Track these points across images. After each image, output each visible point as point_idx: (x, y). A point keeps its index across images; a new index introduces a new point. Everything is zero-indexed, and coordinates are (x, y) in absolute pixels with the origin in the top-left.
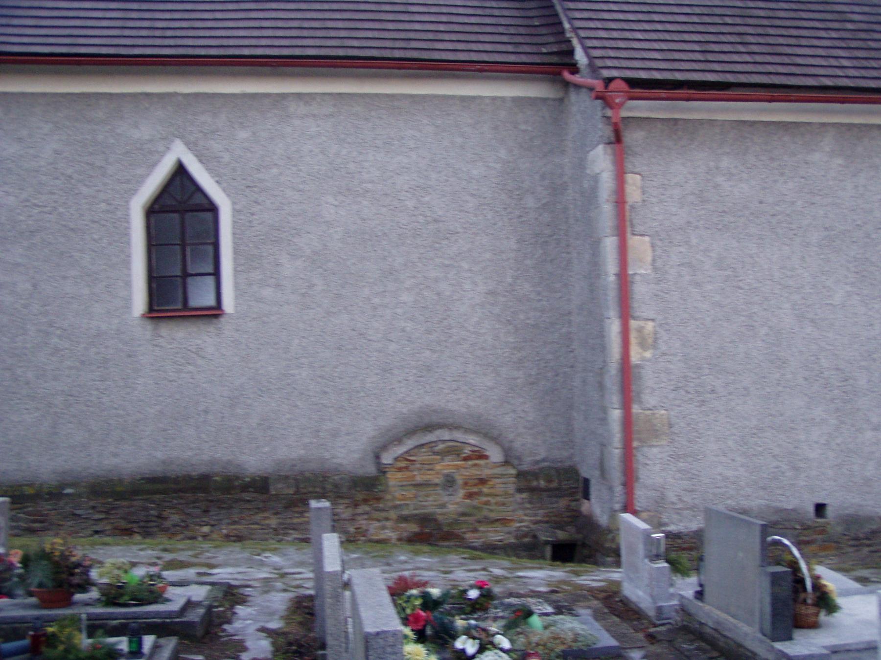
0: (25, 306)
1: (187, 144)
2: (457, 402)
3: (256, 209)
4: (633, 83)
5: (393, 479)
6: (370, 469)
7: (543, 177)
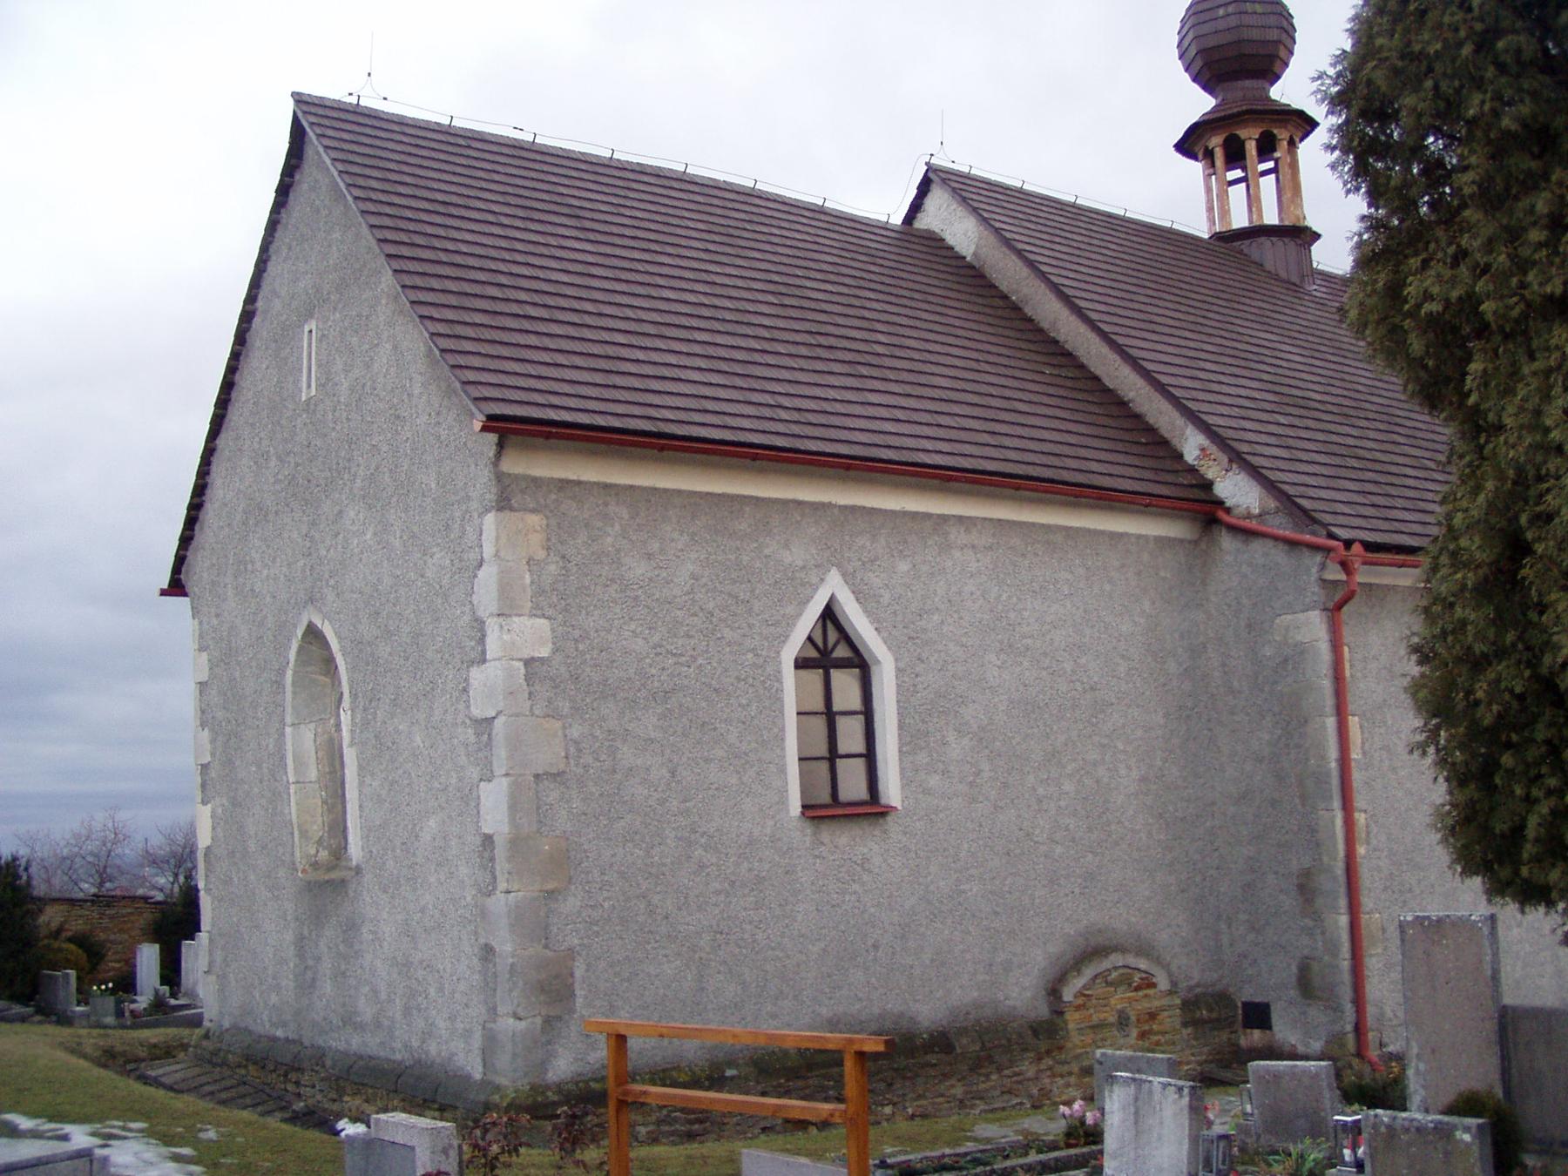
0: (662, 802)
1: (844, 575)
2: (1120, 918)
3: (920, 668)
4: (1370, 547)
5: (1072, 1019)
6: (1043, 1011)
7: (1182, 636)
